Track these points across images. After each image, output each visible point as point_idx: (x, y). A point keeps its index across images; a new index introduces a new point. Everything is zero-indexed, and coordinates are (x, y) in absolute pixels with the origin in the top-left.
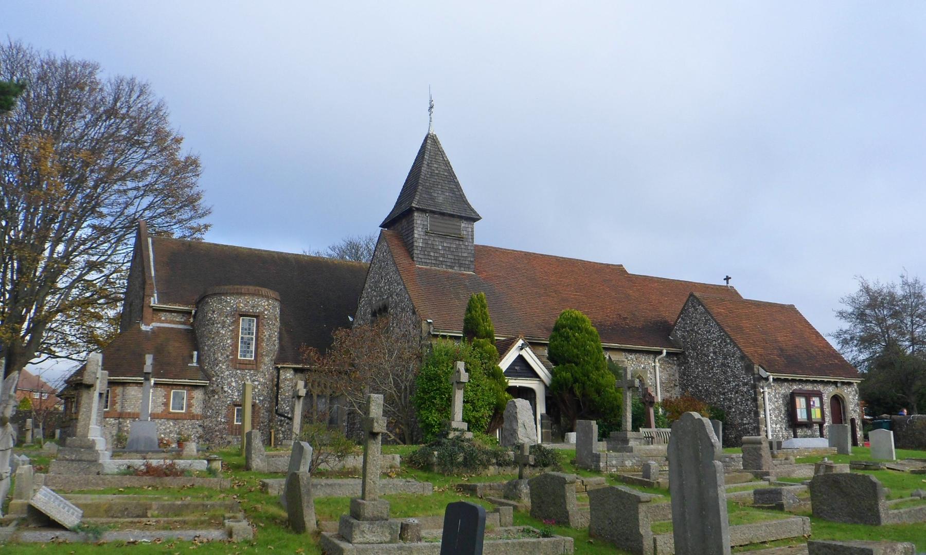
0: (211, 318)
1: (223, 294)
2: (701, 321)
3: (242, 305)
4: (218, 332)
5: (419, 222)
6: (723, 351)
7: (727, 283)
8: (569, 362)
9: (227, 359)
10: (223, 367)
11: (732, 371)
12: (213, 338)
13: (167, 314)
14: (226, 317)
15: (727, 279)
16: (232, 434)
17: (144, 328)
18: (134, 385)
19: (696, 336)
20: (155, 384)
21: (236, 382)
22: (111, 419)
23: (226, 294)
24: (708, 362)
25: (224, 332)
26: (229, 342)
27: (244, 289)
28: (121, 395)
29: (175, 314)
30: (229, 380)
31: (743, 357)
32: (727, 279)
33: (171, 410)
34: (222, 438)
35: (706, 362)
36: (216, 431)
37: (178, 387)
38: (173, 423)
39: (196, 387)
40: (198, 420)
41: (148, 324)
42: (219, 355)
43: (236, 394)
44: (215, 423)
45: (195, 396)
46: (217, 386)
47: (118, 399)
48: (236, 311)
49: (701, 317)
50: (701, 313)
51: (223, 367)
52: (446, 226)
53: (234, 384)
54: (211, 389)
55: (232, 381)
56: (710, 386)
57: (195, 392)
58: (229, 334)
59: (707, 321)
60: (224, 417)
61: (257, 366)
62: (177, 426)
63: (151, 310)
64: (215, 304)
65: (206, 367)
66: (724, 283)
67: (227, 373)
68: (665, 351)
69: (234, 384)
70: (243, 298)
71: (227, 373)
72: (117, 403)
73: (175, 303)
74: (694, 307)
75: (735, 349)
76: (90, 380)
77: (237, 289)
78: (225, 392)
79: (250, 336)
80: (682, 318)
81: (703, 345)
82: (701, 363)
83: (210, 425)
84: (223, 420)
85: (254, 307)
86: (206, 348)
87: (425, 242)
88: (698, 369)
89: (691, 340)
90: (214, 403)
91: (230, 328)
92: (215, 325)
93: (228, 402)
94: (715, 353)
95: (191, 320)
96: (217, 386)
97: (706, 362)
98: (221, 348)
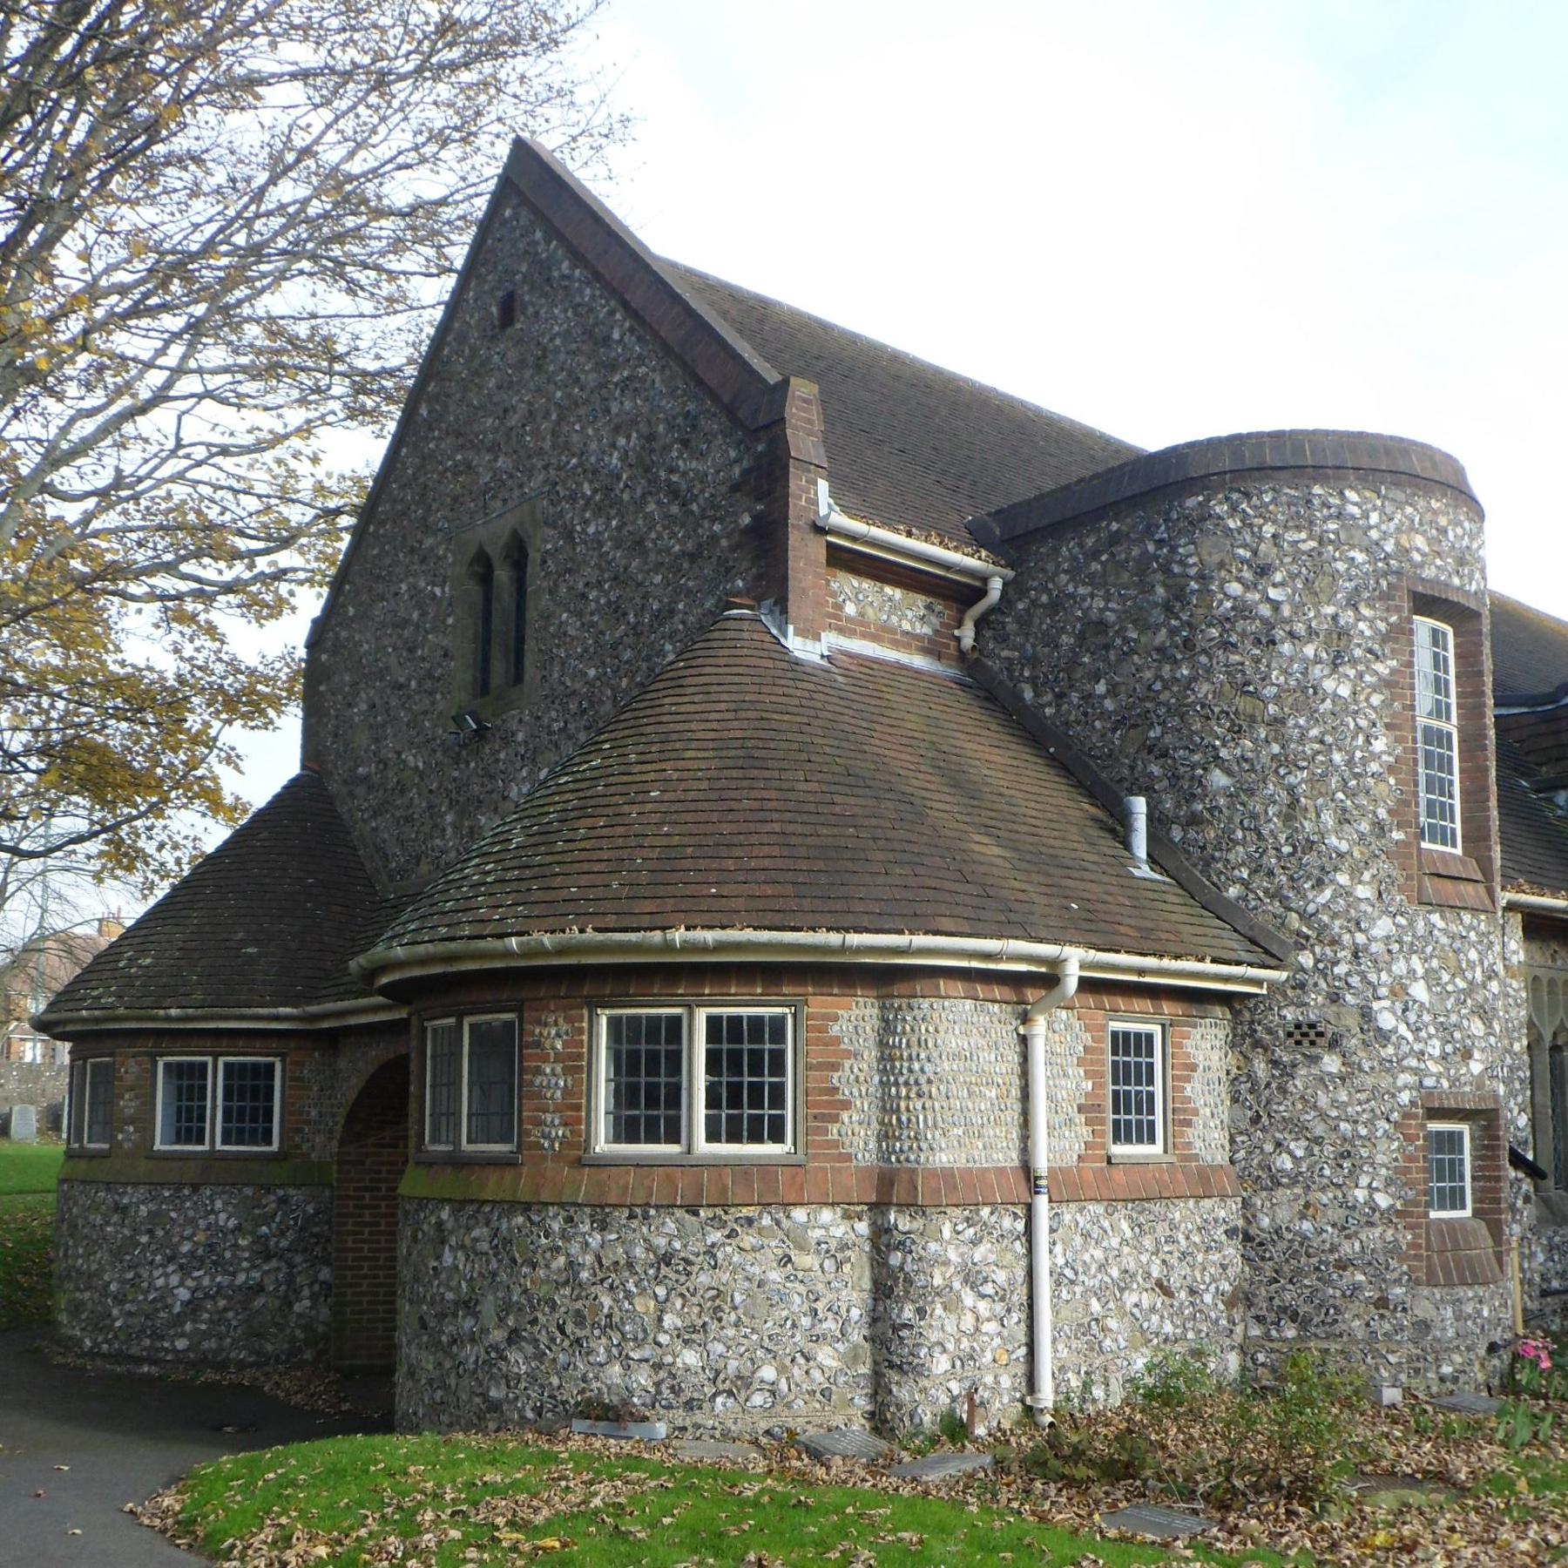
0: (1243, 610)
3: (1420, 541)
4: (1308, 692)
10: (1363, 891)
12: (1277, 722)
16: (1432, 1282)
17: (796, 644)
18: (959, 987)
20: (1086, 985)
21: (1431, 977)
22: (826, 1215)
25: (1345, 691)
26: (1379, 745)
28: (871, 1054)
29: (897, 593)
30: (1400, 967)
34: (1382, 1303)
36: (1342, 1265)
40: (1223, 1197)
42: (1328, 818)
44: (1338, 1214)
53: (1419, 991)
54: (1290, 1014)
55: (1412, 972)
57: (1196, 1033)
58: (1376, 700)
60: (1389, 1182)
62: (1148, 1242)
64: (1269, 530)
65: (1233, 891)
67: (1383, 926)
69: (1419, 991)
70: (1422, 503)
71: (1383, 926)
72: (846, 1105)
73: (926, 528)
76: (18, 933)
83: (1306, 1226)
84: (1383, 1201)
86: (1219, 779)
90: (1323, 1100)
91: (1381, 668)
92: (1286, 648)
93: (1405, 1097)
95: (967, 635)
96: (1334, 998)
98: (1334, 781)
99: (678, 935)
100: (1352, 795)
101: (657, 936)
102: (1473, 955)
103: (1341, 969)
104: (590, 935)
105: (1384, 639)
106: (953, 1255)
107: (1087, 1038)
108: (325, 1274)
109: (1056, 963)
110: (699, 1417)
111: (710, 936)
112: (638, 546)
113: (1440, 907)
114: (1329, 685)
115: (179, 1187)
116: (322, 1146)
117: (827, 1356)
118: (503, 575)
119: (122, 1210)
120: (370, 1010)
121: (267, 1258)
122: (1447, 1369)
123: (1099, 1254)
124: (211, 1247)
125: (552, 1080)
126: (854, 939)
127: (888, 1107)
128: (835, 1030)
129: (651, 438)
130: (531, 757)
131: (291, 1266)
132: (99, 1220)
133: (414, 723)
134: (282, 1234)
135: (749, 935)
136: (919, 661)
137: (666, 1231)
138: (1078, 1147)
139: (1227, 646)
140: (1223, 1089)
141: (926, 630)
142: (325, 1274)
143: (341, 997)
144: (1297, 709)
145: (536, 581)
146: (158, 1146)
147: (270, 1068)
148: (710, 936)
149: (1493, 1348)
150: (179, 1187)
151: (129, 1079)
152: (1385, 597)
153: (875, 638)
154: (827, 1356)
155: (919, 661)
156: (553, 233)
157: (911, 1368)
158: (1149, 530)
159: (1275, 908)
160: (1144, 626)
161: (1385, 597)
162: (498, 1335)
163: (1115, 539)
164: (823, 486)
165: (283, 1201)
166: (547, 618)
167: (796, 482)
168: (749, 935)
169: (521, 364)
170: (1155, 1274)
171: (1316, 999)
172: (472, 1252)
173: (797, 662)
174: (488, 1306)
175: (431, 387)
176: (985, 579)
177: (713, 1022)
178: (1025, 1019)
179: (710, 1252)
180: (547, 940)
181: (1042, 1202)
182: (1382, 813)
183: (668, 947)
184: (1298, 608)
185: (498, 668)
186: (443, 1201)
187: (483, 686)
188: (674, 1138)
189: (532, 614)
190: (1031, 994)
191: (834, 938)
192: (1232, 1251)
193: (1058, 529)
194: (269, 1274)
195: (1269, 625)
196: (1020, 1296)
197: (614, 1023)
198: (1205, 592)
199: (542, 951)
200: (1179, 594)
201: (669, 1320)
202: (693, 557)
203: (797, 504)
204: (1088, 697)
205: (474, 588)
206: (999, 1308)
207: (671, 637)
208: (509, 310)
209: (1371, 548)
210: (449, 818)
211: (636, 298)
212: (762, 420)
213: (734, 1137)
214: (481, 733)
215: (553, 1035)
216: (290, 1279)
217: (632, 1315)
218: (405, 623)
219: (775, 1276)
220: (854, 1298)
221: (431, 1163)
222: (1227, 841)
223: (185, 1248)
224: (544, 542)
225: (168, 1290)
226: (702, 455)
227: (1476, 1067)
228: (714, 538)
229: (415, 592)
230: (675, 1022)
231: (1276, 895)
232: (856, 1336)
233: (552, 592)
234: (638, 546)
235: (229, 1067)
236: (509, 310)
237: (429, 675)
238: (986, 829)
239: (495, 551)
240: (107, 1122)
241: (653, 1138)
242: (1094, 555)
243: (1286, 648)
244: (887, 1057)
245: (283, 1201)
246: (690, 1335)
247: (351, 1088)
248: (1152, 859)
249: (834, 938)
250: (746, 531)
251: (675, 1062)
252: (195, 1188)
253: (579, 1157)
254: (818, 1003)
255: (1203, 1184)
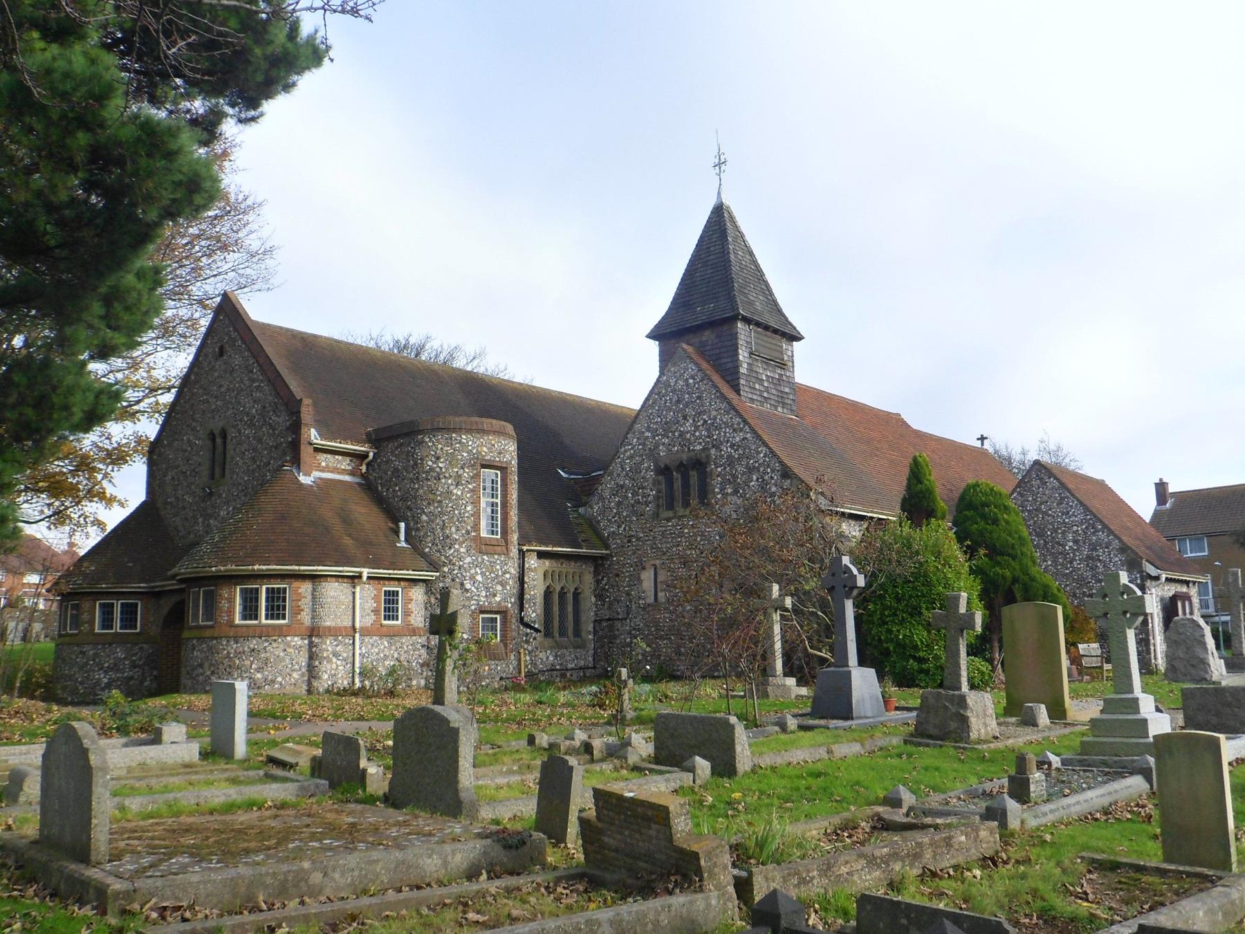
0: (432, 469)
1: (454, 430)
2: (1052, 499)
3: (485, 449)
4: (450, 493)
5: (742, 337)
6: (1090, 540)
7: (982, 444)
8: (1002, 554)
9: (467, 537)
10: (462, 550)
11: (1104, 566)
12: (440, 502)
13: (329, 456)
14: (462, 468)
15: (982, 439)
17: (304, 479)
19: (1043, 518)
20: (369, 578)
22: (296, 639)
23: (458, 430)
24: (1064, 554)
25: (459, 493)
26: (469, 508)
27: (487, 423)
28: (310, 597)
29: (340, 458)
30: (473, 571)
31: (1124, 549)
32: (982, 439)
33: (238, 621)
35: (1061, 553)
37: (392, 583)
38: (388, 642)
39: (414, 582)
40: (420, 636)
41: (308, 474)
42: (453, 529)
43: (484, 594)
45: (414, 598)
46: (453, 580)
47: (306, 603)
48: (477, 458)
49: (1054, 493)
50: (1053, 488)
51: (462, 550)
52: (772, 346)
53: (479, 578)
54: (441, 585)
56: (1067, 585)
57: (413, 590)
59: (1062, 499)
61: (507, 549)
62: (393, 648)
63: (311, 449)
66: (978, 444)
67: (468, 560)
68: (1164, 577)
69: (479, 578)
71: (468, 560)
72: (303, 610)
73: (345, 439)
74: (1041, 479)
75: (1111, 537)
77: (476, 423)
78: (467, 591)
79: (494, 500)
80: (1019, 493)
81: (1056, 532)
82: (1052, 554)
85: (500, 453)
86: (424, 518)
87: (750, 369)
88: (1046, 561)
89: (1035, 523)
91: (470, 486)
92: (443, 481)
93: (473, 607)
94: (1076, 542)
95: (364, 468)
96: (453, 580)
97: (1061, 553)
99: (256, 567)
100: (460, 523)
101: (250, 567)
102: (498, 567)
103: (455, 572)
104: (233, 567)
105: (472, 478)
106: (330, 649)
107: (375, 592)
108: (155, 673)
109: (361, 573)
110: (261, 691)
111: (264, 567)
112: (260, 440)
113: (486, 554)
114: (455, 491)
115: (104, 644)
116: (154, 630)
117: (295, 675)
118: (219, 441)
119: (83, 653)
120: (172, 585)
121: (135, 667)
122: (484, 683)
123: (377, 650)
124: (115, 665)
125: (224, 605)
126: (302, 568)
127: (314, 610)
128: (300, 591)
129: (264, 407)
130: (227, 503)
131: (143, 670)
132: (74, 657)
133: (188, 486)
134: (141, 659)
135: (275, 567)
136: (347, 478)
137: (253, 643)
138: (371, 621)
139: (428, 480)
140: (423, 606)
141: (350, 468)
142: (155, 673)
143: (163, 580)
144: (445, 498)
145: (229, 446)
146: (96, 631)
147: (137, 604)
148: (264, 567)
149: (501, 679)
150: (104, 644)
151: (86, 609)
152: (472, 466)
153: (332, 472)
154: (295, 675)
155: (347, 478)
156: (236, 330)
157: (316, 677)
158: (410, 443)
159: (438, 554)
160: (408, 472)
161: (472, 466)
162: (208, 673)
163: (401, 445)
164: (313, 432)
165: (141, 648)
166: (233, 458)
167: (304, 430)
168: (275, 567)
169: (225, 371)
170: (396, 656)
171: (448, 580)
172: (201, 651)
173: (302, 484)
174: (206, 665)
175: (195, 369)
176: (368, 453)
177: (267, 589)
178: (354, 587)
179: (265, 648)
180: (222, 568)
181: (357, 635)
182: (469, 528)
183: (254, 570)
184: (447, 469)
185: (217, 471)
186: (194, 638)
187: (212, 476)
188: (256, 618)
189: (228, 456)
190: (356, 581)
191: (297, 568)
192: (423, 651)
193: (390, 439)
194: (136, 673)
195: (439, 474)
196: (350, 660)
197: (241, 589)
198: (422, 463)
199: (220, 571)
200: (416, 464)
201: (253, 666)
202: (276, 448)
203: (304, 437)
204: (394, 491)
205: (209, 443)
206: (344, 663)
207: (269, 471)
208: (222, 352)
209: (469, 452)
210: (200, 520)
211: (261, 361)
212: (295, 410)
213: (272, 618)
214: (211, 494)
215: (225, 593)
216: (143, 674)
217: (244, 665)
218: (185, 451)
219: (282, 654)
220: (303, 660)
221: (191, 628)
222: (426, 535)
223: (106, 665)
224: (232, 433)
225: (99, 679)
226: (279, 416)
227: (498, 599)
228: (282, 443)
229: (189, 441)
230: (257, 589)
231: (439, 551)
232: (304, 670)
233: (234, 450)
234: (260, 440)
235: (122, 604)
236: (222, 352)
237: (194, 470)
238: (350, 535)
239: (217, 432)
240: (76, 622)
241: (251, 619)
242: (397, 448)
243: (443, 481)
244: (314, 597)
245: (141, 648)
246: (259, 670)
247: (165, 610)
248: (406, 540)
249: (297, 568)
250: (290, 442)
251: (257, 600)
252: (110, 644)
253: (231, 624)
254: (296, 584)
255: (413, 632)
